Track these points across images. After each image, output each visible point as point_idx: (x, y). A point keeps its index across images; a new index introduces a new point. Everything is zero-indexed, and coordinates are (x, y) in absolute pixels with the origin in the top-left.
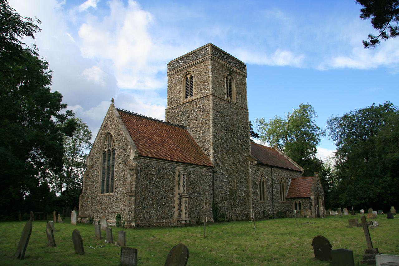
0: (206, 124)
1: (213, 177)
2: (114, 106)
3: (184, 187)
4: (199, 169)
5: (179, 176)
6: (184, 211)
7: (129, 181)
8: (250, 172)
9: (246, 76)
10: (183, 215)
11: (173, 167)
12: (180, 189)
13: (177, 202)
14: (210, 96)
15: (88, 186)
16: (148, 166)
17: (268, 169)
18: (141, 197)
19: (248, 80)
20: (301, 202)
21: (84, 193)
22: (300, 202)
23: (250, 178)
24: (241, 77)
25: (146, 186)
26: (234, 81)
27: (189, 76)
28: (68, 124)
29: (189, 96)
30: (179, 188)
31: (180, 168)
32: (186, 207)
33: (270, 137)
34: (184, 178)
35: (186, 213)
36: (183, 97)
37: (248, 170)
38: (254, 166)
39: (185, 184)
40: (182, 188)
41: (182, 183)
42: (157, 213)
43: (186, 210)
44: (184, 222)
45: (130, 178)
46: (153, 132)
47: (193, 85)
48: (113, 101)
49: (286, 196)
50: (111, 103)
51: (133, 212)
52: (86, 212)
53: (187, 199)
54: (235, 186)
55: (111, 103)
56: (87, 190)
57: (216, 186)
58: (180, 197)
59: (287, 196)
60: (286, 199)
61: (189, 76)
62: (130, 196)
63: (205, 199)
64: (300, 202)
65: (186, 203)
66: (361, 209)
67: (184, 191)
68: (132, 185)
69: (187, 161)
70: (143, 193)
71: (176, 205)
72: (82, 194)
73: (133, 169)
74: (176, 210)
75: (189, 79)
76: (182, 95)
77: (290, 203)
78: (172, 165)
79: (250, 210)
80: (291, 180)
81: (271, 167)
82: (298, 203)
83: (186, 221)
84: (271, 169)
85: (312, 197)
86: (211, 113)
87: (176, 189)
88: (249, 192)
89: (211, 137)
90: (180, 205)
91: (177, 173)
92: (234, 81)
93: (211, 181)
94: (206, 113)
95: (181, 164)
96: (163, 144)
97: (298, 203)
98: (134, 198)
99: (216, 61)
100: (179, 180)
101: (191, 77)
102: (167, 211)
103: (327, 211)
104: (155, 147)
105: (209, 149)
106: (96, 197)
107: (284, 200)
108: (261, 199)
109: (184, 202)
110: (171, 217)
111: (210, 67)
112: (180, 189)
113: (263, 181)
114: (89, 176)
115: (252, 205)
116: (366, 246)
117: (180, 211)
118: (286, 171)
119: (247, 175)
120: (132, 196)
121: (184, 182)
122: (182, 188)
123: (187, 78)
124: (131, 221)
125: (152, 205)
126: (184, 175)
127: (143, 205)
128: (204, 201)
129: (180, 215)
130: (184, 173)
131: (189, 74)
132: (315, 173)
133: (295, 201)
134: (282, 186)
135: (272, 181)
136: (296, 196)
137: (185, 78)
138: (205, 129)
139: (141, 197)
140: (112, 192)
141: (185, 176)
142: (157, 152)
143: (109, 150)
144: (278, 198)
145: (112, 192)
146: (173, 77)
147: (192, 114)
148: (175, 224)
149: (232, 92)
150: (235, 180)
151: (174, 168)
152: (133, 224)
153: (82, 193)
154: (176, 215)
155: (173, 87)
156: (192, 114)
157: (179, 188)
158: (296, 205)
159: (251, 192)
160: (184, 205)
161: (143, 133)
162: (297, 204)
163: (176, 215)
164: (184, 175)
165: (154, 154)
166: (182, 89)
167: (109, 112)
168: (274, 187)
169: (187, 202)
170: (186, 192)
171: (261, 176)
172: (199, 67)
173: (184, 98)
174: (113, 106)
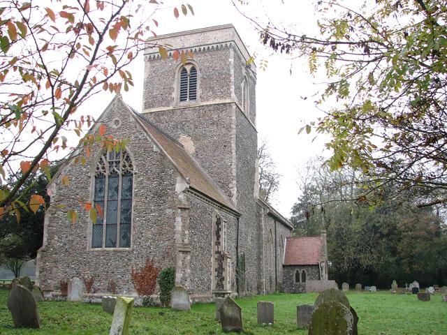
0: (225, 146)
14: (232, 104)
19: (256, 86)
20: (306, 271)
21: (47, 246)
22: (303, 271)
27: (188, 68)
29: (188, 99)
30: (219, 243)
33: (381, 169)
45: (181, 224)
47: (199, 82)
52: (49, 281)
56: (53, 241)
61: (188, 68)
62: (183, 252)
64: (303, 271)
66: (359, 283)
68: (185, 235)
72: (43, 248)
73: (185, 209)
76: (176, 94)
77: (289, 273)
79: (261, 281)
82: (301, 272)
89: (233, 167)
91: (215, 220)
96: (412, 158)
97: (301, 272)
98: (189, 257)
100: (219, 230)
101: (193, 69)
105: (230, 186)
106: (81, 254)
114: (56, 215)
120: (187, 252)
123: (185, 70)
136: (298, 263)
145: (128, 245)
146: (157, 64)
147: (196, 127)
148: (212, 300)
153: (41, 245)
156: (196, 127)
158: (297, 275)
162: (299, 274)
167: (112, 106)
172: (209, 57)
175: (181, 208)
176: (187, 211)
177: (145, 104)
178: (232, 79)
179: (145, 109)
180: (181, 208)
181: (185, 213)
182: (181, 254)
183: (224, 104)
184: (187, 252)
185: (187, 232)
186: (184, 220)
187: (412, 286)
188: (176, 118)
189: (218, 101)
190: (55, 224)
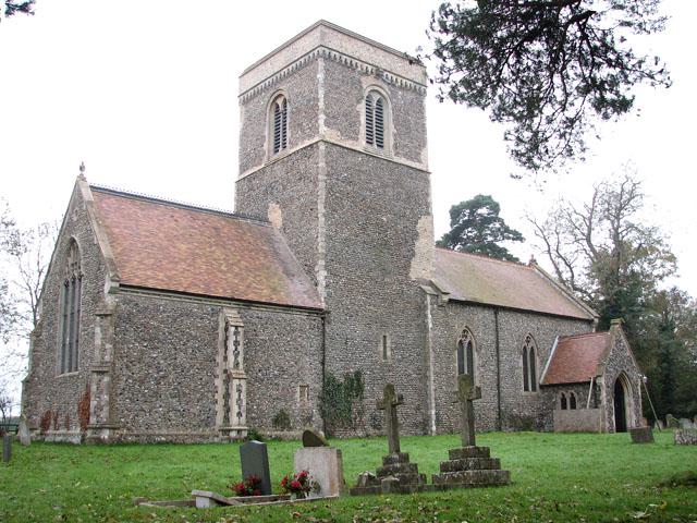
1: (324, 332)
2: (84, 179)
3: (236, 356)
4: (284, 315)
5: (226, 329)
6: (235, 409)
7: (98, 342)
8: (430, 321)
9: (425, 92)
10: (234, 419)
11: (213, 310)
12: (232, 358)
13: (221, 390)
15: (39, 359)
16: (146, 308)
17: (489, 315)
18: (129, 377)
20: (575, 395)
22: (572, 394)
23: (430, 335)
24: (410, 96)
25: (142, 352)
26: (390, 106)
28: (599, 270)
31: (231, 314)
32: (239, 399)
34: (236, 333)
35: (239, 414)
36: (269, 151)
37: (426, 316)
38: (442, 306)
39: (240, 348)
40: (231, 358)
41: (231, 347)
42: (171, 414)
43: (239, 408)
44: (233, 434)
46: (175, 233)
48: (82, 168)
49: (540, 380)
50: (79, 173)
51: (106, 409)
53: (243, 383)
54: (389, 353)
55: (79, 173)
57: (330, 353)
58: (228, 380)
59: (545, 378)
60: (541, 387)
62: (98, 373)
63: (300, 383)
64: (572, 394)
65: (239, 391)
67: (237, 365)
69: (251, 297)
70: (135, 369)
71: (219, 396)
73: (106, 315)
74: (219, 407)
75: (281, 108)
76: (268, 145)
77: (550, 398)
78: (209, 306)
80: (557, 340)
81: (496, 309)
82: (568, 396)
83: (239, 431)
84: (495, 313)
85: (602, 381)
86: (321, 185)
87: (219, 359)
88: (427, 369)
90: (227, 396)
91: (222, 325)
92: (390, 106)
93: (316, 343)
94: (311, 185)
95: (233, 304)
97: (568, 396)
99: (338, 60)
100: (227, 338)
101: (285, 102)
102: (196, 409)
103: (281, 405)
104: (170, 266)
107: (534, 389)
108: (526, 389)
109: (235, 388)
110: (208, 422)
111: (320, 76)
112: (232, 358)
113: (470, 343)
115: (433, 401)
116: (208, 500)
117: (228, 410)
118: (542, 319)
119: (423, 328)
120: (103, 373)
121: (236, 343)
122: (231, 358)
124: (101, 428)
125: (157, 394)
126: (237, 327)
127: (133, 394)
128: (298, 389)
129: (227, 419)
130: (238, 324)
131: (280, 95)
132: (612, 321)
133: (561, 392)
134: (529, 356)
135: (497, 343)
137: (274, 107)
138: (308, 222)
139: (129, 377)
140: (76, 369)
141: (240, 329)
142: (170, 278)
143: (74, 279)
144: (515, 385)
145: (76, 369)
149: (385, 133)
150: (388, 341)
151: (215, 313)
152: (105, 435)
154: (219, 420)
155: (249, 129)
157: (226, 358)
159: (432, 368)
160: (235, 395)
161: (147, 237)
163: (219, 420)
164: (237, 327)
165: (163, 281)
166: (266, 133)
168: (503, 358)
169: (244, 388)
170: (241, 366)
171: (464, 331)
173: (272, 153)
174: (82, 178)
175: (99, 315)
176: (109, 318)
177: (241, 166)
178: (321, 104)
179: (241, 173)
180: (99, 315)
181: (106, 322)
182: (95, 375)
183: (311, 145)
184: (103, 373)
185: (108, 346)
186: (104, 330)
187: (317, 417)
188: (267, 179)
189: (307, 143)
190: (40, 349)
